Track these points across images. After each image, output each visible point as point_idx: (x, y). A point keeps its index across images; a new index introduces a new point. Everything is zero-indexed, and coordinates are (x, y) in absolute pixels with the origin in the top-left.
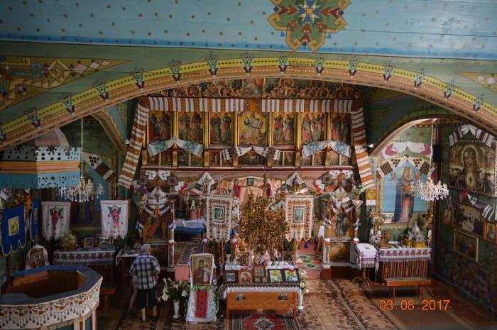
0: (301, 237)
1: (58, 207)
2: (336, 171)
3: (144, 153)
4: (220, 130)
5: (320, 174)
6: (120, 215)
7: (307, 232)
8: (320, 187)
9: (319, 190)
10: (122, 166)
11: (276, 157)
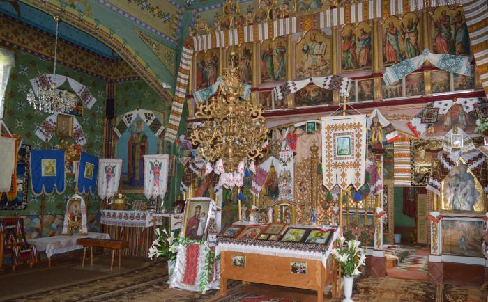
0: (348, 183)
1: (111, 164)
2: (444, 102)
3: (190, 102)
4: (272, 64)
5: (419, 107)
6: (160, 172)
7: (358, 175)
8: (418, 129)
9: (417, 134)
10: (169, 118)
11: (345, 92)
